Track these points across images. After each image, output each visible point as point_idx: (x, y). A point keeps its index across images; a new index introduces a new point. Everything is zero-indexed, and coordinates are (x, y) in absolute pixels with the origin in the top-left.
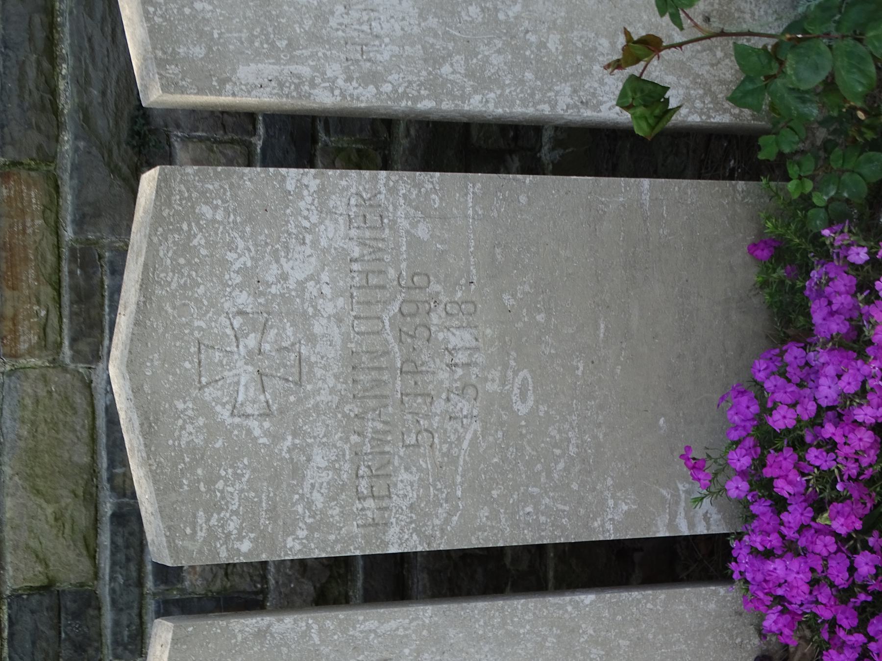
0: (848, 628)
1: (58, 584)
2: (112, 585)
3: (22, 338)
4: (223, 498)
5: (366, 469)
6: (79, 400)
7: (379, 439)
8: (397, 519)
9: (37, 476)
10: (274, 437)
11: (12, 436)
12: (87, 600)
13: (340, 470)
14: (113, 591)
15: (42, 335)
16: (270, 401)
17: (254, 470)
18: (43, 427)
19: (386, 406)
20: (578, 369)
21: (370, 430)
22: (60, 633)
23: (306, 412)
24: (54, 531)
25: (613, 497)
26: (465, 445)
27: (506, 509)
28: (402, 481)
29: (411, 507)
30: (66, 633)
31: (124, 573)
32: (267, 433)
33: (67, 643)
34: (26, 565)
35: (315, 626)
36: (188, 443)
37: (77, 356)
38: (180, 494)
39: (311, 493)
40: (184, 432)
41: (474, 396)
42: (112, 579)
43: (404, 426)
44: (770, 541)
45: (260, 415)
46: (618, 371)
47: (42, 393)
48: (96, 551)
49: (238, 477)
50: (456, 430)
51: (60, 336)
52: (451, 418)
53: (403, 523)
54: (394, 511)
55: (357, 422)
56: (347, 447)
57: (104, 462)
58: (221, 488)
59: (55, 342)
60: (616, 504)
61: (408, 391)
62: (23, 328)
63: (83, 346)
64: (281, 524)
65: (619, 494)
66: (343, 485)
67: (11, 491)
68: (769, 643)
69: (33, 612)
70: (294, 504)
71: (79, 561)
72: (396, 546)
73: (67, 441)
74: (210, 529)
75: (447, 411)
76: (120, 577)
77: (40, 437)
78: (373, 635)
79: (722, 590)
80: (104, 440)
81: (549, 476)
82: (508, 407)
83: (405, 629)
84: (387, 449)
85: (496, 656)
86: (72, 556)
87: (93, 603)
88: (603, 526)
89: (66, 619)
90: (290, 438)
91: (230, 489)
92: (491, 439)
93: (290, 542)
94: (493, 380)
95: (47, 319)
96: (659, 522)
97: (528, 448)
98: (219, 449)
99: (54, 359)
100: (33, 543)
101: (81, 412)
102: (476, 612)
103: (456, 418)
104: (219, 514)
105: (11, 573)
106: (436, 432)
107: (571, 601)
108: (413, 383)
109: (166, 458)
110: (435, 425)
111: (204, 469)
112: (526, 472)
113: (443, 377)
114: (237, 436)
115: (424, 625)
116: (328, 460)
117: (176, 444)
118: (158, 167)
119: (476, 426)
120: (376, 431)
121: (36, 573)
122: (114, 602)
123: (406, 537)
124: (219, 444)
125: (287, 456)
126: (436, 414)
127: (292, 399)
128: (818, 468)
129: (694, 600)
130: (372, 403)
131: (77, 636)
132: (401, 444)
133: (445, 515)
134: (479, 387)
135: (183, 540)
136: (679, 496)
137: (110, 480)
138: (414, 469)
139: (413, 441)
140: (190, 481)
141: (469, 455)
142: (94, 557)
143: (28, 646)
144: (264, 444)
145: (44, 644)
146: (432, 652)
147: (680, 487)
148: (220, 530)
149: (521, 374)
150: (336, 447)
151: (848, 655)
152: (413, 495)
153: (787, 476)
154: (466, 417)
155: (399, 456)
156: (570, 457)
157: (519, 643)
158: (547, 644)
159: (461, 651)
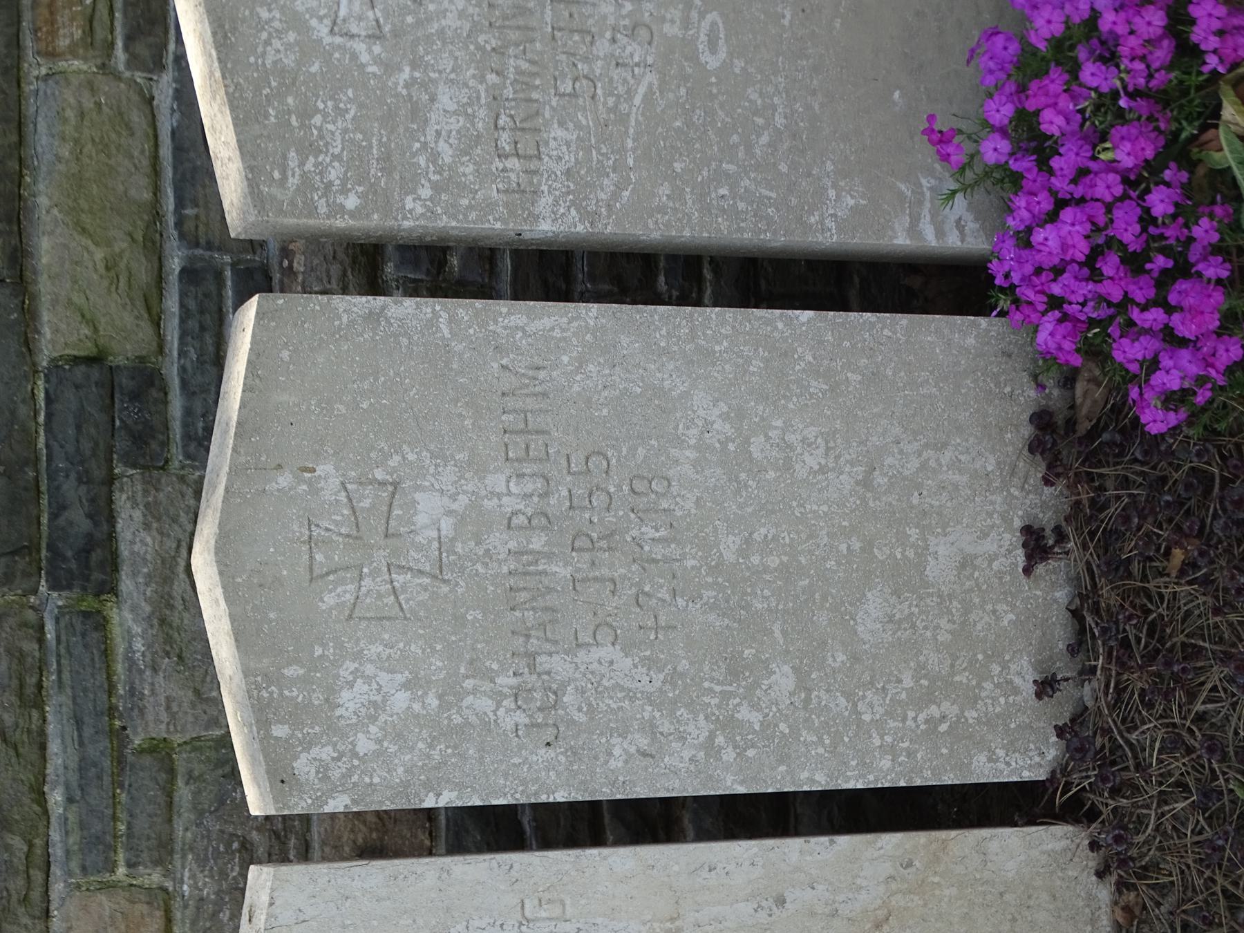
0: (1143, 301)
1: (111, 358)
2: (182, 361)
3: (61, 32)
4: (321, 137)
5: (508, 119)
6: (137, 118)
7: (524, 82)
8: (550, 186)
9: (82, 211)
10: (387, 65)
11: (48, 157)
12: (147, 380)
13: (474, 117)
14: (183, 369)
15: (88, 28)
16: (381, 20)
17: (361, 106)
18: (89, 147)
19: (533, 41)
20: (784, 17)
21: (512, 69)
22: (114, 421)
23: (428, 39)
24: (106, 283)
25: (834, 186)
26: (638, 100)
27: (693, 189)
28: (555, 139)
29: (568, 173)
30: (121, 420)
31: (198, 346)
32: (377, 60)
33: (123, 433)
34: (68, 325)
35: (444, 315)
36: (275, 63)
37: (134, 61)
38: (265, 126)
39: (436, 142)
40: (269, 48)
41: (648, 39)
42: (182, 354)
43: (556, 68)
44: (1039, 203)
45: (369, 37)
46: (838, 25)
47: (88, 104)
48: (160, 318)
49: (341, 113)
50: (625, 81)
51: (112, 33)
52: (617, 64)
53: (557, 193)
54: (546, 176)
55: (495, 57)
56: (482, 88)
57: (169, 203)
58: (318, 124)
59: (105, 40)
60: (838, 197)
61: (562, 24)
62: (63, 18)
63: (141, 49)
64: (398, 178)
65: (842, 184)
66: (478, 136)
67: (48, 228)
68: (1048, 397)
69: (77, 387)
70: (414, 155)
71: (137, 325)
72: (549, 221)
73: (121, 169)
74: (304, 175)
75: (613, 55)
76: (192, 351)
77: (86, 160)
78: (520, 334)
79: (983, 321)
80: (170, 175)
81: (749, 148)
82: (694, 58)
83: (563, 330)
84: (535, 95)
85: (684, 378)
86: (128, 319)
87: (157, 382)
88: (822, 222)
89: (122, 401)
90: (407, 69)
91: (330, 127)
92: (671, 95)
93: (409, 203)
94: (673, 22)
95: (94, 10)
96: (897, 226)
97: (720, 113)
98: (315, 74)
99: (104, 64)
100: (78, 299)
101: (139, 133)
102: (656, 317)
103: (624, 65)
104: (316, 157)
105: (48, 336)
106: (599, 80)
107: (781, 315)
108: (567, 15)
109: (246, 79)
110: (598, 72)
111: (296, 98)
112: (718, 143)
113: (607, 11)
114: (339, 60)
115: (586, 327)
116: (458, 103)
117: (260, 61)
118: (256, 298)
119: (651, 78)
120: (519, 72)
121: (82, 337)
122: (184, 384)
123: (562, 211)
124: (315, 68)
125: (404, 92)
126: (598, 58)
127: (410, 19)
128: (1096, 90)
129: (946, 331)
130: (514, 35)
131: (136, 423)
132: (552, 91)
133: (612, 188)
134: (654, 27)
135: (269, 186)
136: (922, 193)
137: (179, 224)
138: (571, 125)
139: (569, 90)
140: (278, 112)
141: (643, 114)
142: (159, 325)
143: (71, 432)
144: (374, 74)
145: (92, 430)
146: (599, 363)
147: (924, 181)
148: (318, 178)
149: (710, 17)
150: (468, 87)
151: (1145, 343)
152: (570, 159)
153: (1056, 104)
154: (637, 65)
155: (551, 107)
156: (776, 129)
157: (714, 364)
158: (751, 368)
159: (638, 366)
